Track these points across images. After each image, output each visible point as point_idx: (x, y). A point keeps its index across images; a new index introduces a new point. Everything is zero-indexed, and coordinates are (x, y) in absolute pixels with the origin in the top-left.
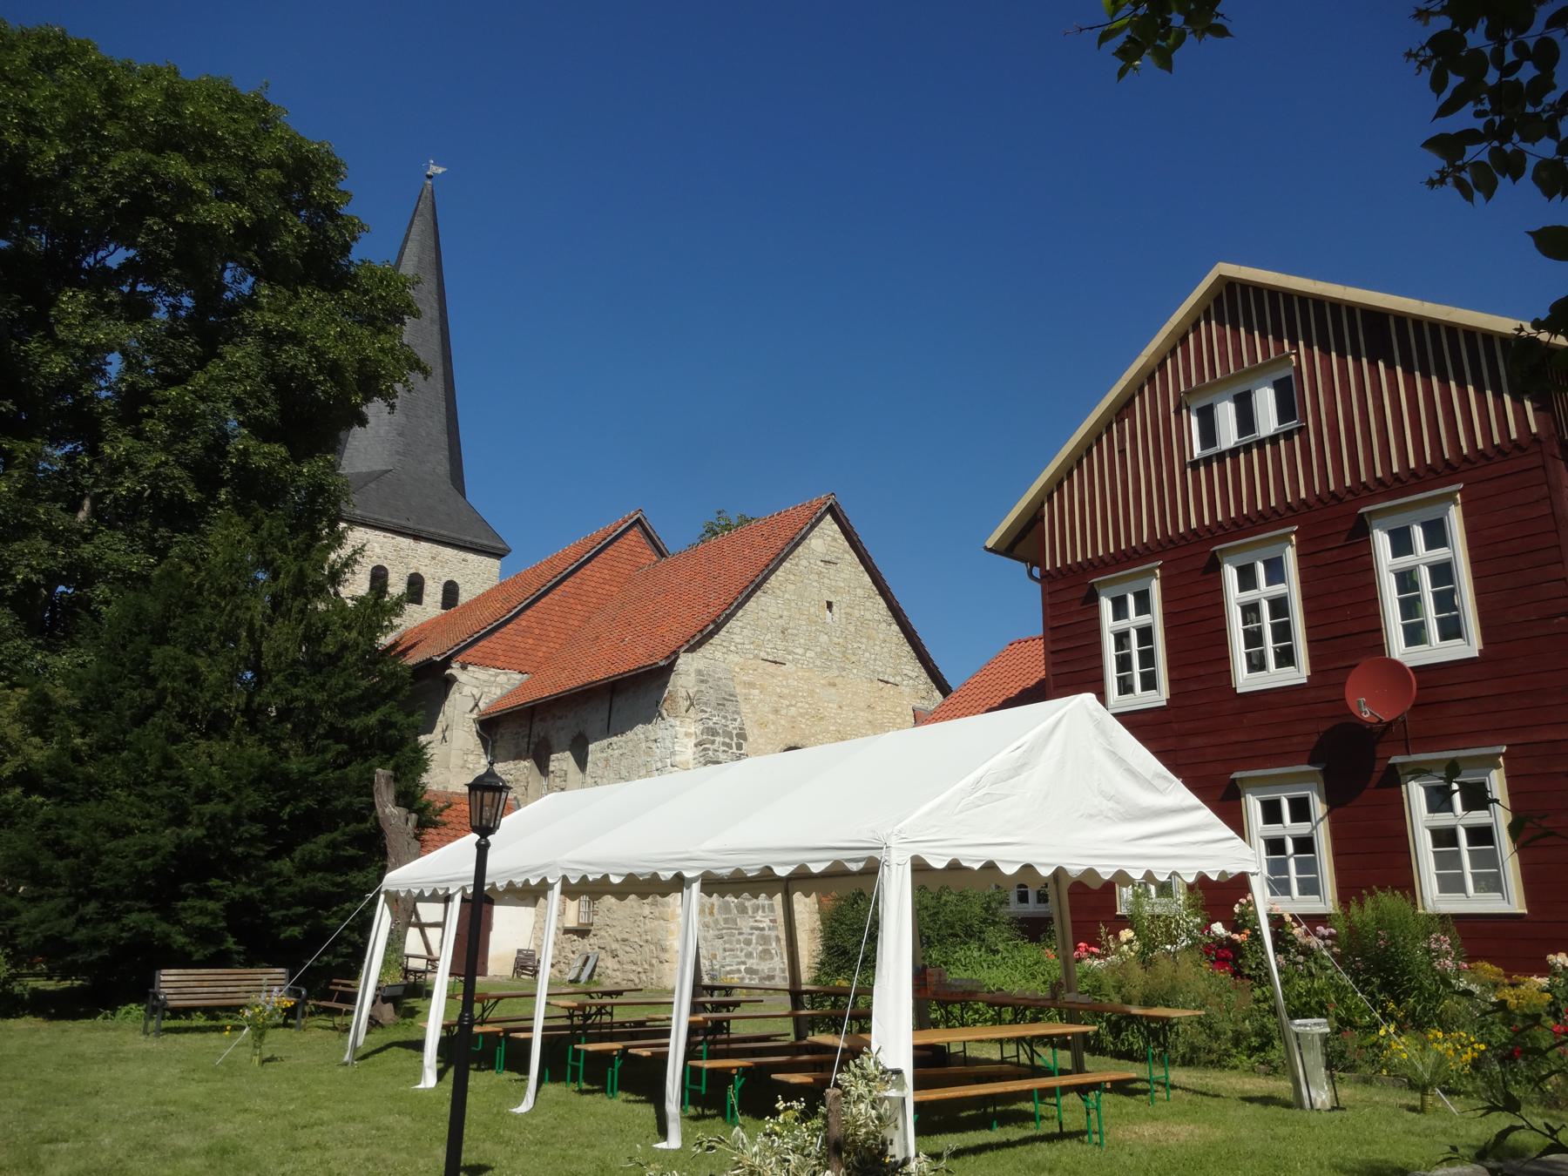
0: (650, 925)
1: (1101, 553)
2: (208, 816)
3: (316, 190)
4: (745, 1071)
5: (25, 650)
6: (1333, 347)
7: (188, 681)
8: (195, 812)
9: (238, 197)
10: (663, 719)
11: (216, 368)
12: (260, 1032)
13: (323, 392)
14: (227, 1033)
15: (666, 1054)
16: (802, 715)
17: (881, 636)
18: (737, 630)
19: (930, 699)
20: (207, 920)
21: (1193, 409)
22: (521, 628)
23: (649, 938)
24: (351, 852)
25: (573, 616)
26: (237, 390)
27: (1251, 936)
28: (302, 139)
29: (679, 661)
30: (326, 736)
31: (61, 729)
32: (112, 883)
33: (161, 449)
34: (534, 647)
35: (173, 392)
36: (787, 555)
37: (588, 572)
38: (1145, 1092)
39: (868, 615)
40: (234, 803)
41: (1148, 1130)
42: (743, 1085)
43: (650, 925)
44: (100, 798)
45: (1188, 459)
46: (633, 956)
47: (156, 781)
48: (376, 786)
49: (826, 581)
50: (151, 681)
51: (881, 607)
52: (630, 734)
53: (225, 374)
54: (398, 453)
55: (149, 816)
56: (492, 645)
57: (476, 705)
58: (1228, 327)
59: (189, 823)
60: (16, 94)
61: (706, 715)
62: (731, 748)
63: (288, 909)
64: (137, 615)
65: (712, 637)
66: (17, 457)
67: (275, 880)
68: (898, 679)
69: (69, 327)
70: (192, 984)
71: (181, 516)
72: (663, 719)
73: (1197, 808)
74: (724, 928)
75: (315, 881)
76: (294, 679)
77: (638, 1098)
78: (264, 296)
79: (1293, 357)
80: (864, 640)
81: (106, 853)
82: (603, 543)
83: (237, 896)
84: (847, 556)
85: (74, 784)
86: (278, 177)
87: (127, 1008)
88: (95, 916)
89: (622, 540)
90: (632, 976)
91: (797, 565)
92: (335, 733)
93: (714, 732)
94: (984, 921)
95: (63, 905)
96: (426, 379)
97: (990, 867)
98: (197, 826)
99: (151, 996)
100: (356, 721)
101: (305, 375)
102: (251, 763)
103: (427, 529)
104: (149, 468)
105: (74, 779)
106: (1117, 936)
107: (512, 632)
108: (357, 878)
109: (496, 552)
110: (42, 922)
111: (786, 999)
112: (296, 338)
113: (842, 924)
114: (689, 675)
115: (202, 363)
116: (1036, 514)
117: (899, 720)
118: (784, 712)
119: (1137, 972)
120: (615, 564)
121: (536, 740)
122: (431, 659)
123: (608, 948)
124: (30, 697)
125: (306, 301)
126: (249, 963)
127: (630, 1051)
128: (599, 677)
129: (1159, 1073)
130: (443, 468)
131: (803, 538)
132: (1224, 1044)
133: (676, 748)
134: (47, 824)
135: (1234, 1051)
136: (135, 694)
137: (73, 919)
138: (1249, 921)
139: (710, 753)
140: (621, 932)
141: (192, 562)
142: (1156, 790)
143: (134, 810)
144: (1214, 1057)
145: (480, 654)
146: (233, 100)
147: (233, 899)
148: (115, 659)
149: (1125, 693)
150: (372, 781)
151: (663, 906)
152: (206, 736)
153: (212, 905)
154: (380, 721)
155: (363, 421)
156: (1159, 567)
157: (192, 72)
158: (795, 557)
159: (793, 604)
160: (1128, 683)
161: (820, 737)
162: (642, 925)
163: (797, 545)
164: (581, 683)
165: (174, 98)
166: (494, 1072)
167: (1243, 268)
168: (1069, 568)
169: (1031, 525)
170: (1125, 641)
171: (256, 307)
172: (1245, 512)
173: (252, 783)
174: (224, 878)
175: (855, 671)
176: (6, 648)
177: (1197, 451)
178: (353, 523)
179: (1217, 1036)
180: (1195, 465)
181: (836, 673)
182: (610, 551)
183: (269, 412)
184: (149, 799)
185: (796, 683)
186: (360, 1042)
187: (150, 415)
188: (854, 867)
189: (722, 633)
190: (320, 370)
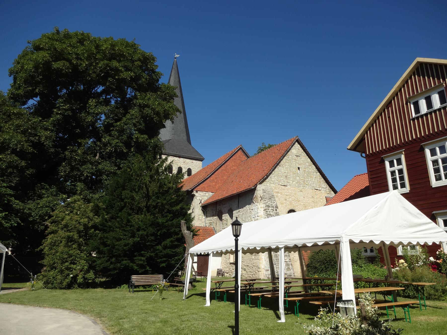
0: (254, 261)
1: (384, 148)
2: (140, 235)
3: (149, 66)
4: (300, 301)
5: (87, 193)
6: (431, 76)
7: (131, 199)
8: (137, 234)
9: (131, 70)
10: (254, 203)
11: (128, 116)
12: (161, 291)
13: (155, 120)
14: (153, 292)
15: (278, 296)
16: (293, 200)
17: (314, 176)
18: (273, 177)
19: (330, 194)
20: (142, 262)
21: (412, 103)
22: (211, 180)
23: (254, 265)
24: (176, 243)
25: (225, 176)
26: (134, 121)
27: (443, 261)
28: (145, 52)
29: (257, 187)
30: (167, 212)
31: (102, 213)
32: (118, 253)
33: (116, 139)
34: (215, 185)
35: (118, 123)
36: (285, 155)
37: (228, 164)
38: (418, 307)
39: (310, 171)
40: (146, 231)
41: (423, 318)
42: (299, 305)
43: (254, 261)
44: (113, 231)
45: (411, 118)
46: (250, 270)
47: (126, 226)
48: (181, 225)
49: (297, 161)
50: (122, 200)
51: (314, 168)
52: (245, 208)
53: (131, 117)
54: (173, 134)
55: (125, 235)
56: (204, 185)
57: (201, 202)
58: (421, 77)
59: (135, 237)
60: (74, 50)
61: (266, 202)
62: (274, 211)
63: (162, 259)
64: (117, 183)
65: (266, 180)
66: (82, 144)
67: (158, 251)
68: (321, 188)
69: (92, 109)
70: (140, 279)
71: (122, 156)
72: (254, 203)
73: (431, 223)
74: (276, 262)
75: (168, 251)
76: (158, 198)
77: (267, 309)
78: (139, 95)
79: (444, 84)
80: (310, 178)
81: (117, 245)
82: (232, 155)
83: (149, 256)
84: (303, 154)
85: (106, 228)
86: (139, 63)
87: (123, 286)
88: (115, 262)
89: (236, 154)
90: (250, 276)
91: (288, 157)
92: (169, 212)
93: (269, 207)
94: (357, 258)
95: (107, 259)
96: (180, 114)
97: (371, 242)
98: (138, 238)
99: (130, 282)
100: (174, 208)
101: (150, 116)
102: (149, 220)
103: (182, 154)
104: (114, 144)
105: (106, 226)
106: (398, 261)
107: (209, 181)
108: (178, 250)
109: (201, 160)
110: (102, 264)
111: (302, 281)
112: (147, 106)
113: (314, 260)
114: (260, 191)
115: (124, 115)
116: (362, 138)
117: (322, 200)
118: (288, 200)
119: (409, 273)
120: (235, 161)
121: (218, 211)
122: (188, 190)
123: (243, 268)
124: (93, 206)
125: (148, 96)
126: (153, 273)
127: (265, 295)
128: (235, 193)
129: (422, 302)
130: (185, 138)
131: (290, 150)
132: (440, 293)
133: (258, 211)
134: (101, 238)
135: (443, 295)
136: (119, 203)
137: (109, 263)
138: (442, 256)
139: (268, 212)
140: (246, 263)
141: (130, 168)
142: (418, 218)
143: (122, 234)
144: (437, 297)
145: (201, 188)
146: (127, 44)
147: (148, 256)
148: (113, 194)
149: (395, 189)
150: (180, 224)
151: (258, 256)
152: (137, 214)
153: (143, 258)
154: (180, 208)
155: (164, 127)
156: (404, 151)
157: (116, 38)
158: (288, 155)
159: (288, 169)
160: (396, 186)
161: (299, 206)
162: (252, 261)
163: (288, 152)
164: (230, 195)
165: (113, 46)
166: (224, 302)
167: (425, 58)
168: (374, 153)
169: (361, 140)
170: (394, 174)
171: (137, 99)
172: (431, 132)
173: (150, 226)
174: (145, 251)
175: (307, 187)
176: (83, 193)
177: (414, 115)
178: (169, 155)
179: (437, 291)
180: (413, 119)
181: (302, 188)
182: (234, 157)
183: (142, 127)
184: (125, 231)
185: (291, 191)
186: (187, 294)
187: (113, 130)
188: (332, 243)
189: (269, 178)
190: (154, 114)
